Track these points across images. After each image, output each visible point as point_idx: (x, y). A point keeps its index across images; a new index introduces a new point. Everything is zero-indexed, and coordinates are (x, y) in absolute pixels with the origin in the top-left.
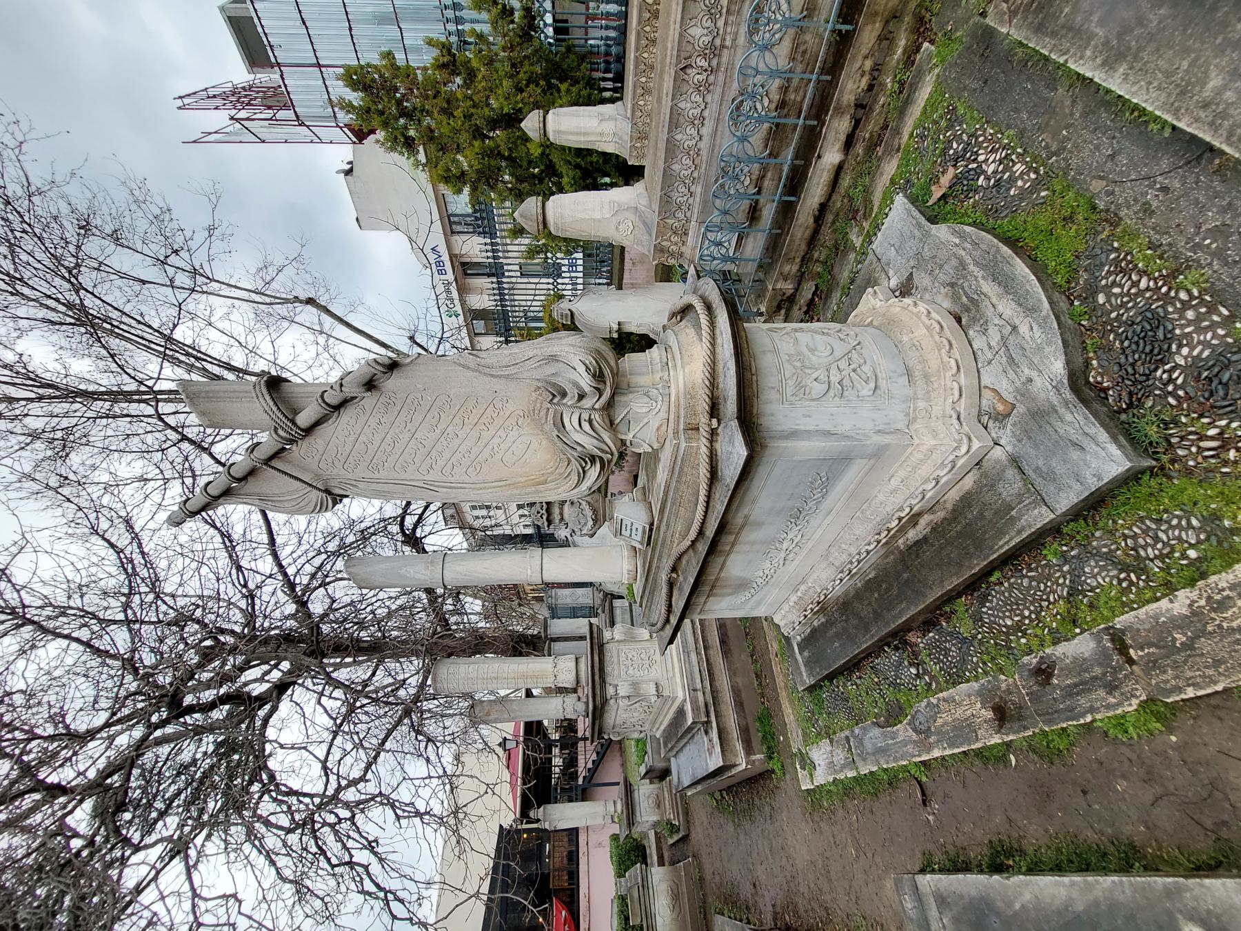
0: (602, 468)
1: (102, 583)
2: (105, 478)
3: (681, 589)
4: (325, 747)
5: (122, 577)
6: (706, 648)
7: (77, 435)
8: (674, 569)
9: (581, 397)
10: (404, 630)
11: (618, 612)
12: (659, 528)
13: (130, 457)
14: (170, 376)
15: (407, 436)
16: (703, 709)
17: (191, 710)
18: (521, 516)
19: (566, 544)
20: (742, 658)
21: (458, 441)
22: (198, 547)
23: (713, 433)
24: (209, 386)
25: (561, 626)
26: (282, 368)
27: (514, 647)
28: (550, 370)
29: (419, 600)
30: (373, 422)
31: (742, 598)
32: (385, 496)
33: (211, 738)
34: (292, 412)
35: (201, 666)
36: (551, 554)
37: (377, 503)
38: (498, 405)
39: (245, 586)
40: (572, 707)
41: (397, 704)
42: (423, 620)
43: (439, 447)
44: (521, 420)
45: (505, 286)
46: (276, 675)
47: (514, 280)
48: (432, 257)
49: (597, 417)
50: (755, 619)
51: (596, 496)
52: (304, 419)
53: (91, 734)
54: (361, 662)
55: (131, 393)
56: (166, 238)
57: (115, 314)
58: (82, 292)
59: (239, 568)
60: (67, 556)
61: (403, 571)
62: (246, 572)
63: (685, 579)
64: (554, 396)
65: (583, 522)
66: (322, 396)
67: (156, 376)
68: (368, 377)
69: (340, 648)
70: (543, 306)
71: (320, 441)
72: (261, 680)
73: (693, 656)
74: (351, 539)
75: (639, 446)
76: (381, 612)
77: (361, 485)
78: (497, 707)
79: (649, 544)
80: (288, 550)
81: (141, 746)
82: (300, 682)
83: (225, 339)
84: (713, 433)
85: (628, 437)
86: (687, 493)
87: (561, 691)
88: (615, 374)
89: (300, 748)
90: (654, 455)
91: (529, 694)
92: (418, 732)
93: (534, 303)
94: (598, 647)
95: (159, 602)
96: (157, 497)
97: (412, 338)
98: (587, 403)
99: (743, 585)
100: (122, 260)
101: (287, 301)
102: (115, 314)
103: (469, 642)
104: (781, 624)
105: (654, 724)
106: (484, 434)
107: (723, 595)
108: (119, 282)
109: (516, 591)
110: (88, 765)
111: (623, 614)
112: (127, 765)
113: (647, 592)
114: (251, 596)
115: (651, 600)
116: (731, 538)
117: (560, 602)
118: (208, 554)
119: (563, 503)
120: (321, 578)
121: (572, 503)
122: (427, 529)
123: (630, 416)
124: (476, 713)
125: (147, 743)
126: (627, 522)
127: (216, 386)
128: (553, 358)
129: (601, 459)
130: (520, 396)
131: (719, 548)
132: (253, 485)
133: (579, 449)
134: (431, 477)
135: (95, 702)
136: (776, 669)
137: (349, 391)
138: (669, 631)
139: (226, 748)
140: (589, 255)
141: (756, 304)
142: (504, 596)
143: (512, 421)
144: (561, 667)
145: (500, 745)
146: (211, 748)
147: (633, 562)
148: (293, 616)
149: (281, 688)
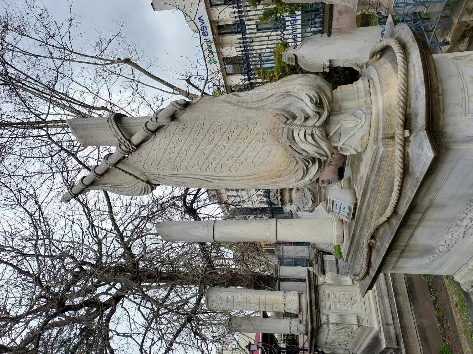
0: (320, 166)
1: (22, 233)
2: (22, 172)
3: (378, 251)
4: (141, 337)
5: (32, 230)
6: (396, 295)
7: (7, 148)
8: (373, 237)
9: (306, 119)
10: (187, 267)
11: (327, 264)
12: (361, 207)
13: (33, 160)
14: (54, 113)
15: (194, 148)
16: (394, 339)
17: (69, 308)
18: (258, 196)
19: (291, 216)
20: (426, 304)
21: (225, 151)
22: (70, 213)
23: (406, 141)
24: (82, 119)
25: (286, 271)
26: (115, 105)
27: (255, 283)
28: (285, 102)
29: (195, 249)
30: (174, 140)
31: (426, 260)
32: (175, 184)
33: (78, 326)
34: (129, 135)
35: (73, 283)
36: (283, 224)
37: (170, 188)
38: (251, 126)
39: (97, 236)
40: (296, 327)
41: (184, 314)
42: (199, 262)
43: (213, 155)
44: (265, 136)
45: (247, 40)
46: (114, 291)
47: (253, 35)
48: (199, 24)
49: (317, 132)
50: (437, 277)
51: (315, 185)
52: (136, 139)
53: (16, 319)
54: (163, 286)
55: (33, 123)
56: (46, 28)
57: (23, 77)
58: (6, 65)
59: (93, 226)
60: (4, 217)
61: (189, 231)
62: (97, 229)
63: (382, 244)
64: (288, 119)
65: (305, 202)
66: (146, 125)
67: (47, 113)
68: (172, 113)
69: (150, 277)
70: (274, 52)
71: (144, 152)
72: (106, 293)
73: (386, 300)
74: (155, 210)
75: (347, 150)
76: (173, 255)
77: (167, 178)
78: (246, 322)
79: (353, 218)
80: (120, 215)
81: (44, 327)
82: (127, 296)
83: (80, 88)
84: (406, 141)
85: (339, 145)
86: (384, 183)
87: (287, 315)
88: (331, 102)
89: (128, 337)
90: (358, 157)
91: (265, 315)
92: (196, 333)
93: (268, 50)
94: (315, 288)
95: (51, 244)
96: (49, 183)
97: (188, 80)
98: (310, 123)
99: (428, 251)
100: (25, 44)
101: (113, 62)
102: (23, 77)
103: (227, 278)
104: (461, 282)
105: (355, 345)
106: (241, 145)
107: (412, 257)
108: (23, 57)
109: (255, 246)
110: (16, 336)
111: (331, 265)
112: (37, 338)
113: (352, 252)
114: (99, 243)
115: (354, 258)
116: (418, 216)
117: (286, 254)
118: (76, 217)
119: (291, 189)
120: (139, 233)
121: (298, 189)
122: (200, 204)
123: (341, 130)
124: (233, 325)
125: (47, 326)
126: (337, 202)
127: (85, 121)
128: (288, 94)
129: (320, 160)
130: (265, 120)
131: (409, 223)
132: (107, 179)
133: (304, 154)
134: (209, 173)
135: (21, 301)
136: (457, 317)
137: (162, 121)
138: (368, 280)
139: (86, 333)
140: (306, 12)
141: (443, 35)
142: (247, 248)
143: (259, 136)
144: (289, 299)
145: (247, 347)
146: (78, 332)
147: (341, 230)
148: (122, 256)
149: (117, 299)
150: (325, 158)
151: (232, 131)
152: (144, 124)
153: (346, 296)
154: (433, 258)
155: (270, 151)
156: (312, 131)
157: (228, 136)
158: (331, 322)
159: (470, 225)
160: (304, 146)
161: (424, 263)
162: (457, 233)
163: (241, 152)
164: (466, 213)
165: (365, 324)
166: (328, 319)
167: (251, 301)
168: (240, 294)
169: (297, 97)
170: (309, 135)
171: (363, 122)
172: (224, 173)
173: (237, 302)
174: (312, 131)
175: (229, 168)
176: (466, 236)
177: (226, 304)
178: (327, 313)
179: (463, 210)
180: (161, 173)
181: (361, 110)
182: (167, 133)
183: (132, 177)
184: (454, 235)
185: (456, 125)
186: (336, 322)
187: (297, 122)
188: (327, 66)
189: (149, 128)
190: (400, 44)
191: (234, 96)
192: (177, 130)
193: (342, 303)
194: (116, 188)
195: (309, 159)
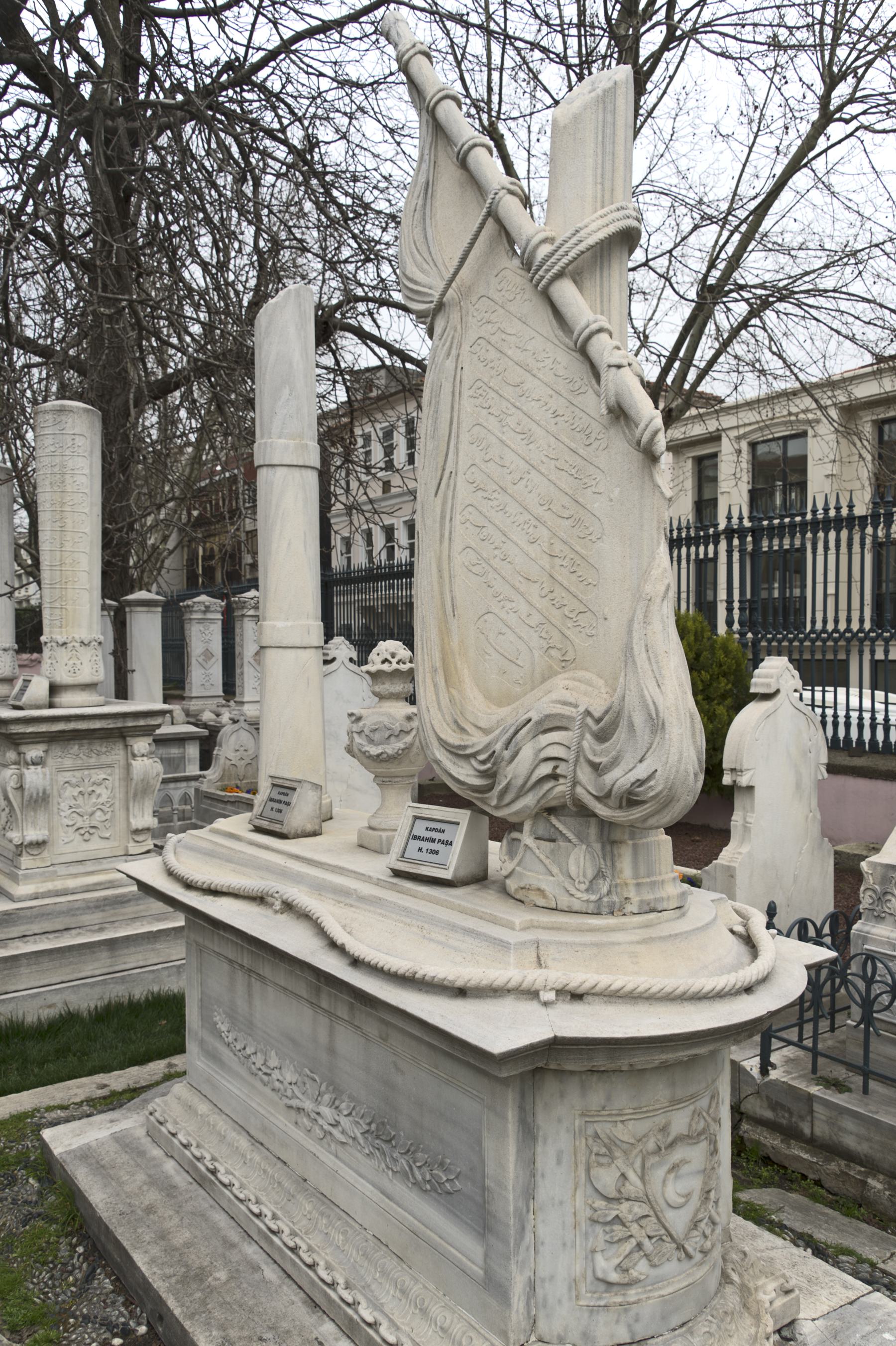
9: (596, 767)
43: (513, 508)
49: (561, 788)
52: (566, 292)
64: (598, 721)
65: (377, 737)
68: (632, 413)
98: (585, 775)
119: (412, 700)
129: (490, 788)
133: (507, 754)
150: (494, 802)
151: (574, 569)
152: (606, 325)
153: (99, 813)
154: (230, 1039)
155: (518, 662)
156: (565, 777)
157: (563, 555)
158: (25, 771)
159: (320, 1121)
160: (527, 754)
161: (217, 1019)
162: (300, 1095)
163: (517, 585)
164: (350, 1114)
165: (26, 861)
166: (34, 764)
167: (68, 547)
168: (86, 510)
169: (648, 749)
170: (556, 767)
171: (579, 895)
172: (459, 529)
173: (63, 504)
174: (565, 777)
175: (473, 545)
176: (293, 1113)
177: (56, 470)
178: (50, 761)
179: (357, 1109)
180: (466, 347)
181: (609, 892)
182: (577, 386)
183: (455, 262)
184: (293, 1087)
185: (562, 1096)
186: (27, 786)
187: (588, 742)
188: (738, 779)
189: (595, 339)
190: (768, 974)
191: (663, 588)
192: (585, 416)
193: (80, 800)
194: (425, 199)
195: (494, 764)
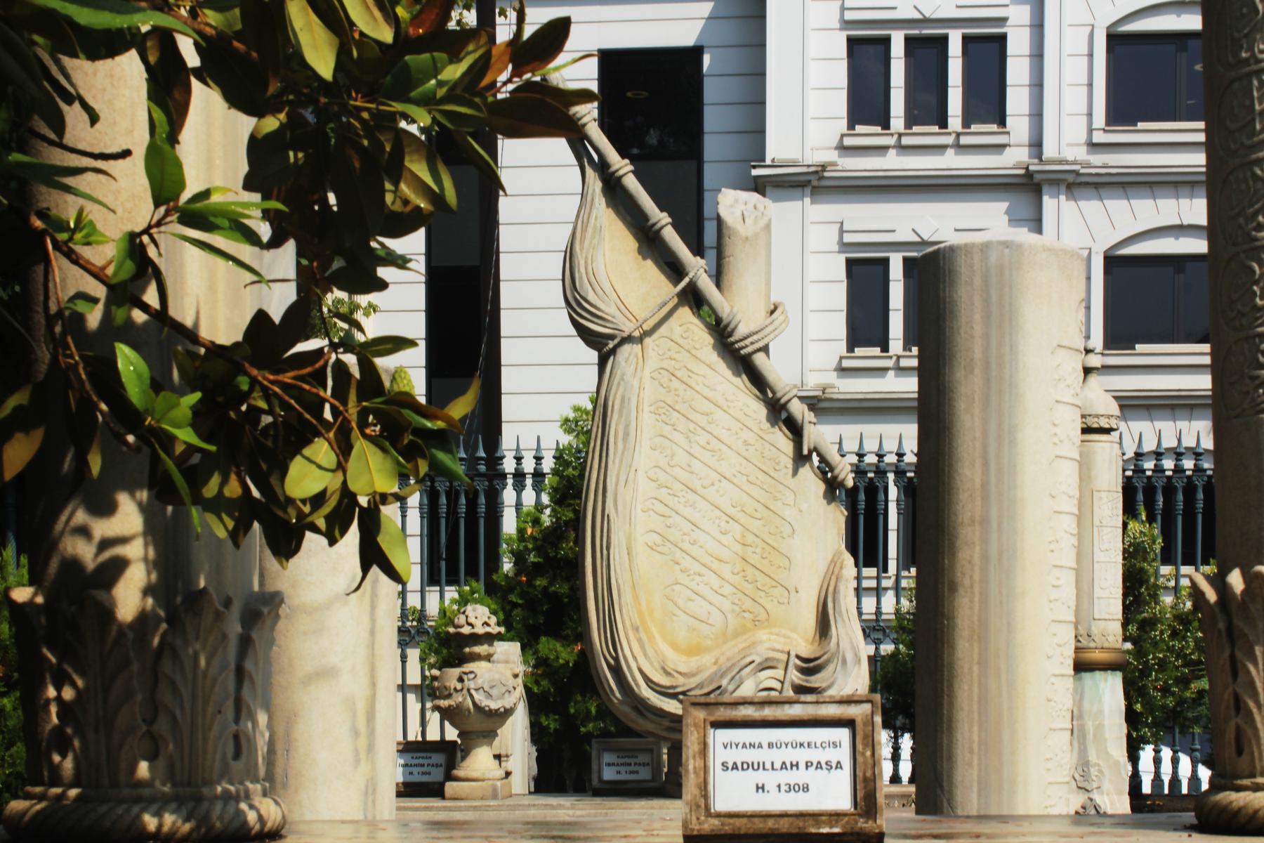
65: (494, 692)
180: (647, 373)
